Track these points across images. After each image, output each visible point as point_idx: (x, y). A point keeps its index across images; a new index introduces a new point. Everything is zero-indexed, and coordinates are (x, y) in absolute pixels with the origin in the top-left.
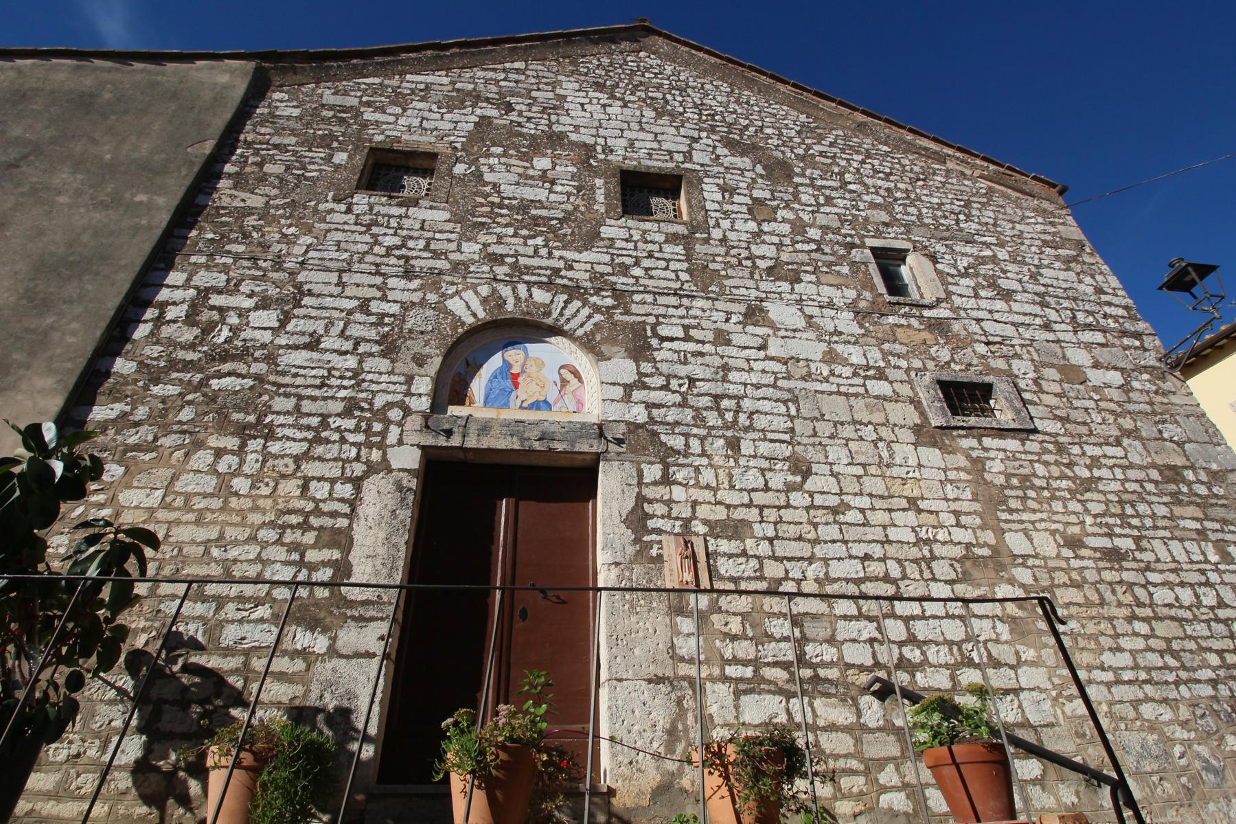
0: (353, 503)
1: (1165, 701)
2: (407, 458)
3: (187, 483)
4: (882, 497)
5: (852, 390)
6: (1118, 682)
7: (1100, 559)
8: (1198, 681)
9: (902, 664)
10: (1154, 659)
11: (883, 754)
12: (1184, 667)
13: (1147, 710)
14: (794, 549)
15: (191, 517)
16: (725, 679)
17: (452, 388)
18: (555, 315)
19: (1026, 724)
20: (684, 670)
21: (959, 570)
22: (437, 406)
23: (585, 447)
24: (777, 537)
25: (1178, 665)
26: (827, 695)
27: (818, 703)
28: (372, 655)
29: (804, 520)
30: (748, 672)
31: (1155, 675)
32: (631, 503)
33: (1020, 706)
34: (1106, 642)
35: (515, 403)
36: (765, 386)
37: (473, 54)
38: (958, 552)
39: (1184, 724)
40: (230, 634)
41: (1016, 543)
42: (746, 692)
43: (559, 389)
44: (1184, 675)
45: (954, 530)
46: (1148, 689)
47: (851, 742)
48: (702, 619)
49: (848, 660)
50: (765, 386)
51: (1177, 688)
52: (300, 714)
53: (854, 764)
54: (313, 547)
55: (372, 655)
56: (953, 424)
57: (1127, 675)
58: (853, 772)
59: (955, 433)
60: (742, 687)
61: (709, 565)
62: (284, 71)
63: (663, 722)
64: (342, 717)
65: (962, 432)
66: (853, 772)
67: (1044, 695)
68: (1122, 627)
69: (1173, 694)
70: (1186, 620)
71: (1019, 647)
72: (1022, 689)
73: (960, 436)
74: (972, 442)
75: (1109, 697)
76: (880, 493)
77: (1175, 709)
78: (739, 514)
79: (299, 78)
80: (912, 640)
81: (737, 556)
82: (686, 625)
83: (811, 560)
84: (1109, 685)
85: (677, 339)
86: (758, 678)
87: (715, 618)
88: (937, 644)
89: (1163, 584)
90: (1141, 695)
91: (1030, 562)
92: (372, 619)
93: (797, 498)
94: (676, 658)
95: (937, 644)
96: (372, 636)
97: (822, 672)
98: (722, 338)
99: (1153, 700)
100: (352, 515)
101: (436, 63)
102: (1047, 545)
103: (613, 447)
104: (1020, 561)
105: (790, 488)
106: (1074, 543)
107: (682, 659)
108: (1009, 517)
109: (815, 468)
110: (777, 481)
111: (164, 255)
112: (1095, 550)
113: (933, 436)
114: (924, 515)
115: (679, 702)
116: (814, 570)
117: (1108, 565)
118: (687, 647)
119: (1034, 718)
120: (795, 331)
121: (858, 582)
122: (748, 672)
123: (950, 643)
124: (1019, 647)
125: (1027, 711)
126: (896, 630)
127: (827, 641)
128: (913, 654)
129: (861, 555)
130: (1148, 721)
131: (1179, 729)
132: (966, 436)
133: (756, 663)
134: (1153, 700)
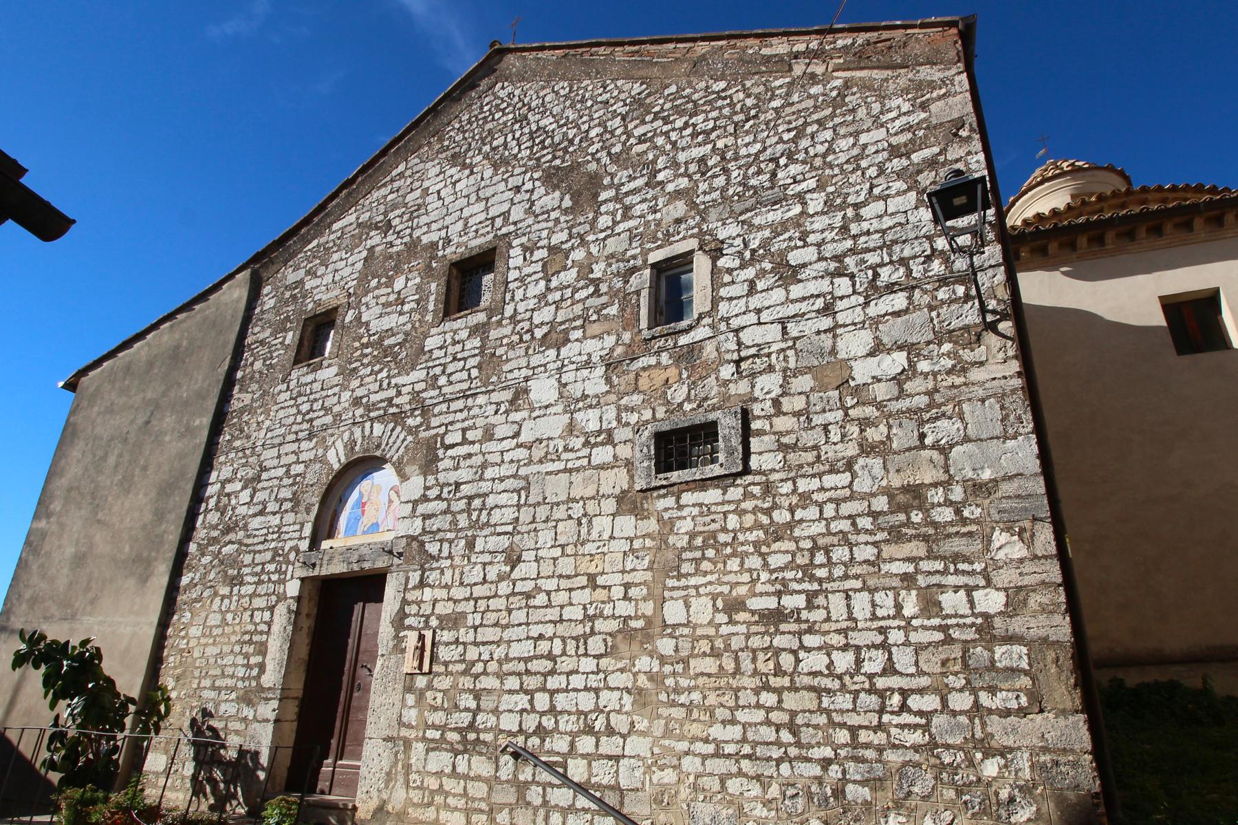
0: (269, 624)
1: (758, 778)
2: (293, 588)
3: (211, 622)
4: (568, 577)
5: (578, 463)
6: (717, 755)
7: (756, 623)
8: (808, 760)
9: (540, 731)
10: (768, 734)
11: (504, 801)
12: (798, 744)
13: (734, 786)
14: (490, 634)
15: (211, 641)
16: (424, 739)
17: (324, 527)
18: (359, 442)
19: (616, 788)
20: (404, 732)
21: (610, 644)
22: (314, 543)
23: (380, 564)
24: (481, 625)
25: (792, 740)
26: (481, 754)
27: (475, 759)
28: (268, 721)
29: (503, 607)
30: (437, 735)
31: (760, 751)
32: (397, 607)
33: (617, 772)
34: (722, 714)
35: (359, 532)
36: (508, 477)
37: (370, 176)
38: (613, 625)
39: (767, 803)
40: (223, 707)
41: (674, 612)
42: (433, 749)
43: (380, 512)
44: (793, 751)
45: (619, 604)
46: (746, 765)
47: (486, 789)
48: (421, 695)
49: (502, 727)
50: (508, 477)
51: (778, 766)
52: (242, 752)
53: (483, 806)
54: (253, 655)
55: (268, 721)
56: (653, 484)
57: (730, 749)
58: (482, 811)
59: (655, 494)
60: (432, 745)
61: (432, 651)
62: (265, 266)
63: (386, 769)
64: (256, 755)
65: (663, 491)
66: (482, 811)
67: (640, 763)
68: (747, 697)
69: (770, 770)
70: (828, 691)
71: (635, 717)
72: (624, 756)
73: (659, 497)
74: (670, 502)
75: (701, 769)
76: (568, 573)
77: (765, 787)
78: (461, 608)
79: (275, 268)
80: (552, 710)
81: (451, 643)
82: (411, 699)
83: (498, 643)
84: (704, 757)
85: (457, 444)
86: (443, 738)
87: (429, 694)
88: (569, 713)
89: (820, 648)
90: (734, 769)
91: (710, 748)
92: (271, 699)
93: (504, 588)
94: (401, 724)
95: (569, 713)
96: (268, 710)
97: (482, 736)
98: (489, 435)
99: (746, 775)
100: (268, 633)
101: (349, 202)
102: (702, 610)
103: (396, 561)
104: (669, 631)
105: (501, 578)
106: (734, 606)
107: (404, 725)
108: (676, 584)
109: (525, 556)
110: (492, 574)
111: (207, 465)
112: (753, 612)
113: (634, 503)
114: (599, 590)
115: (396, 755)
116: (499, 652)
117: (762, 629)
118: (411, 715)
119: (624, 783)
120: (546, 407)
121: (527, 660)
122: (437, 735)
123: (580, 713)
124: (635, 717)
125: (621, 775)
126: (542, 701)
127: (492, 712)
128: (548, 722)
129: (536, 635)
130: (730, 795)
131: (760, 806)
132: (664, 496)
133: (443, 728)
134: (746, 775)
